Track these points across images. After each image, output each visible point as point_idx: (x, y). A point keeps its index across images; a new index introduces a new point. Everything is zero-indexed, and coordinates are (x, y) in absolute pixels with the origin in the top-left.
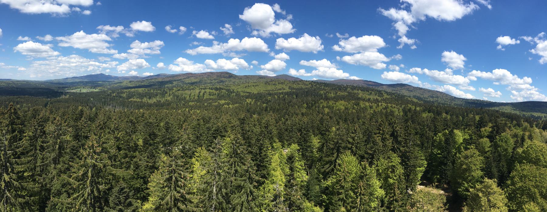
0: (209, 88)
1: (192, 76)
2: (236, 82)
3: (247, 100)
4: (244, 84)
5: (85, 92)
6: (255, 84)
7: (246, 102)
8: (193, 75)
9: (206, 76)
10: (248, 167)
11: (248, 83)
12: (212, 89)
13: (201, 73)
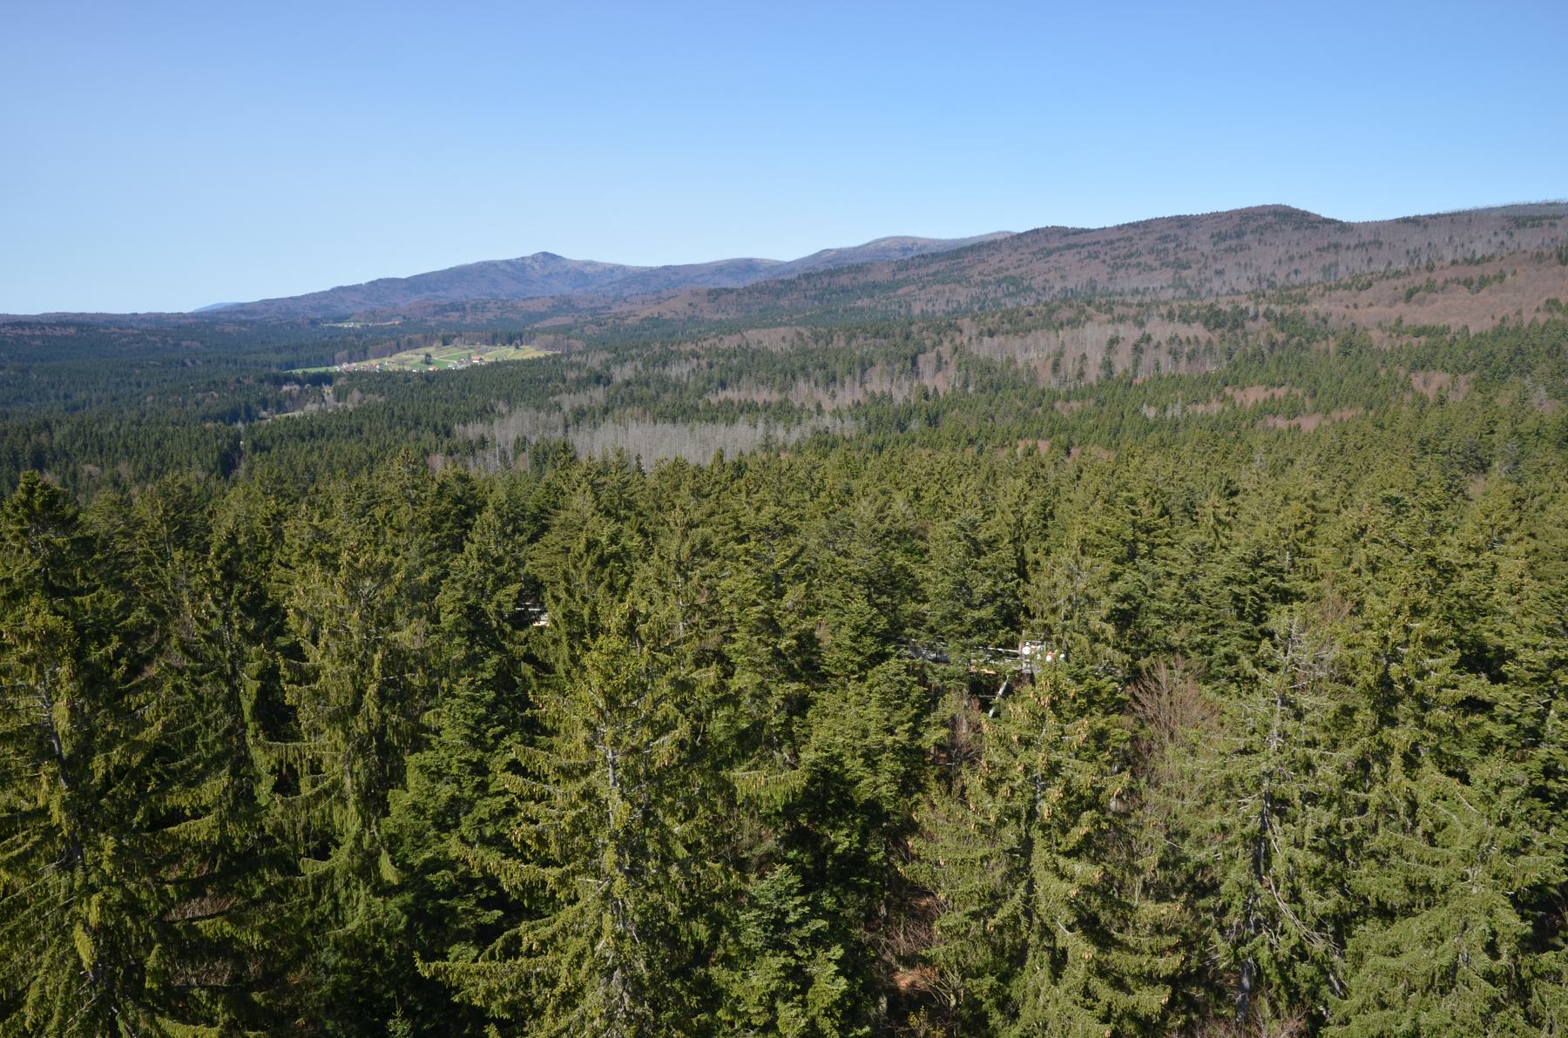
0: (1171, 315)
1: (1069, 247)
2: (1342, 268)
3: (1417, 380)
4: (1398, 274)
5: (452, 365)
6: (1475, 272)
7: (1408, 397)
8: (1073, 240)
9: (1150, 239)
10: (1108, 593)
11: (1430, 268)
12: (1186, 319)
13: (1119, 228)
